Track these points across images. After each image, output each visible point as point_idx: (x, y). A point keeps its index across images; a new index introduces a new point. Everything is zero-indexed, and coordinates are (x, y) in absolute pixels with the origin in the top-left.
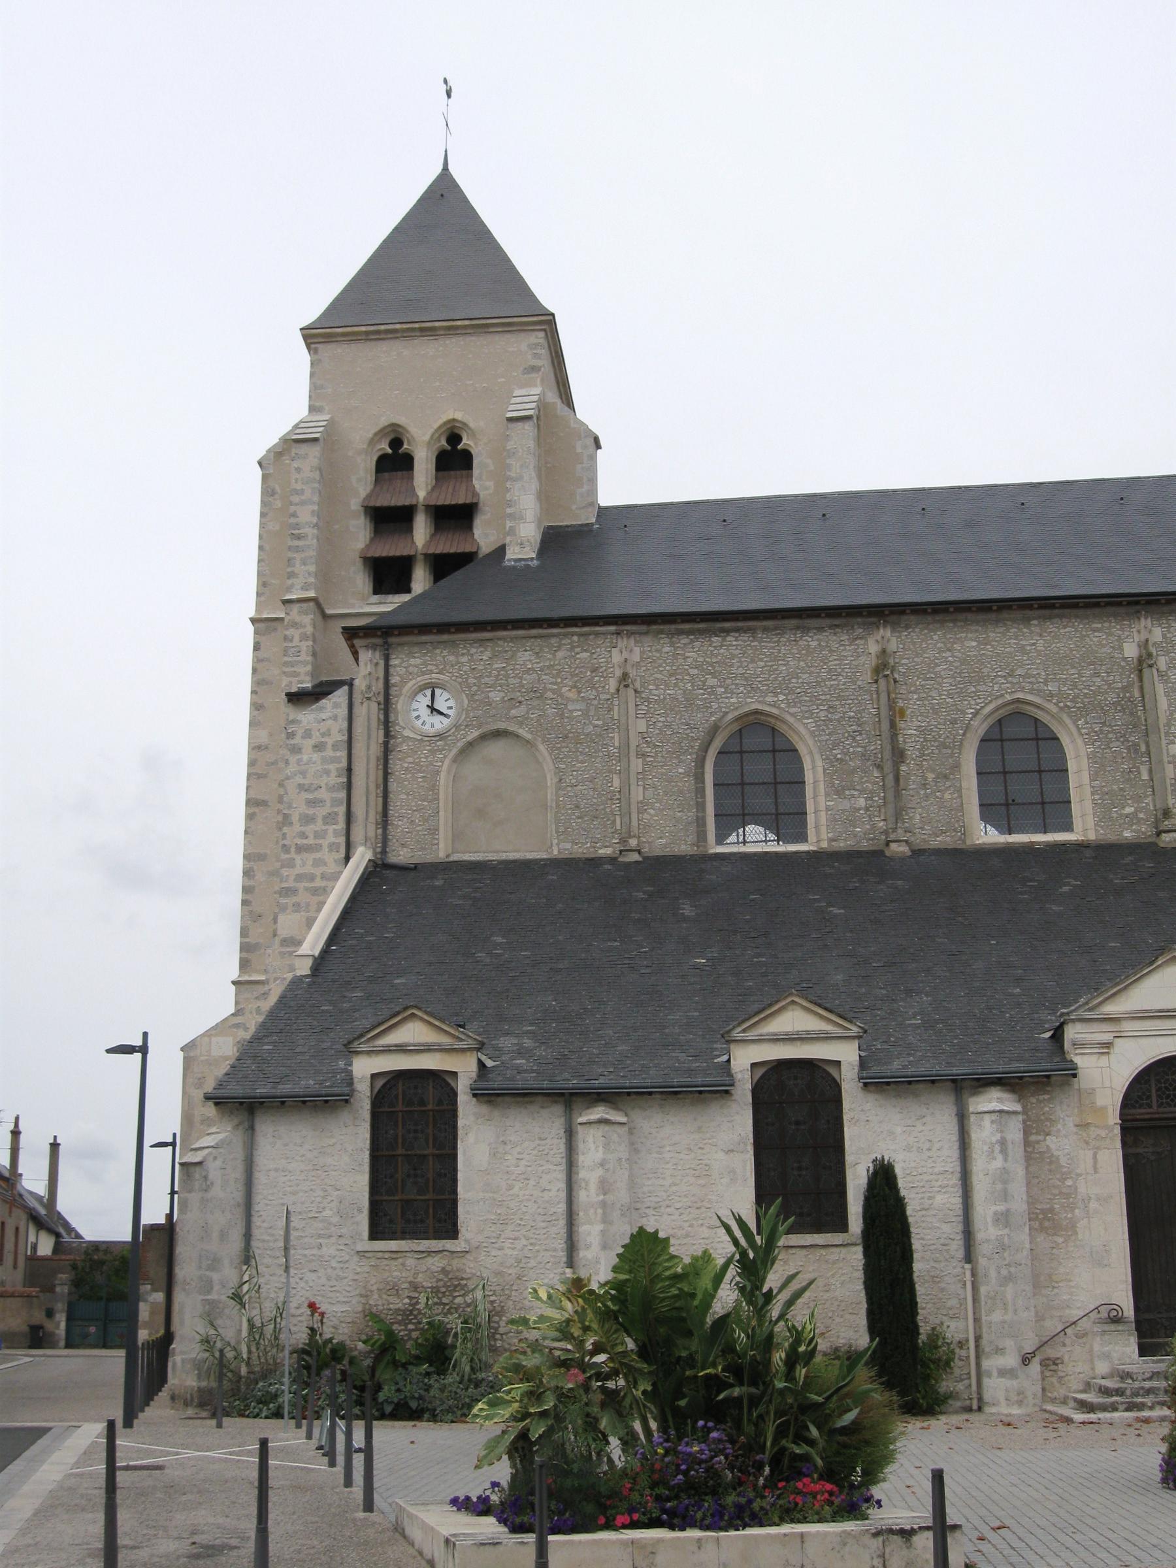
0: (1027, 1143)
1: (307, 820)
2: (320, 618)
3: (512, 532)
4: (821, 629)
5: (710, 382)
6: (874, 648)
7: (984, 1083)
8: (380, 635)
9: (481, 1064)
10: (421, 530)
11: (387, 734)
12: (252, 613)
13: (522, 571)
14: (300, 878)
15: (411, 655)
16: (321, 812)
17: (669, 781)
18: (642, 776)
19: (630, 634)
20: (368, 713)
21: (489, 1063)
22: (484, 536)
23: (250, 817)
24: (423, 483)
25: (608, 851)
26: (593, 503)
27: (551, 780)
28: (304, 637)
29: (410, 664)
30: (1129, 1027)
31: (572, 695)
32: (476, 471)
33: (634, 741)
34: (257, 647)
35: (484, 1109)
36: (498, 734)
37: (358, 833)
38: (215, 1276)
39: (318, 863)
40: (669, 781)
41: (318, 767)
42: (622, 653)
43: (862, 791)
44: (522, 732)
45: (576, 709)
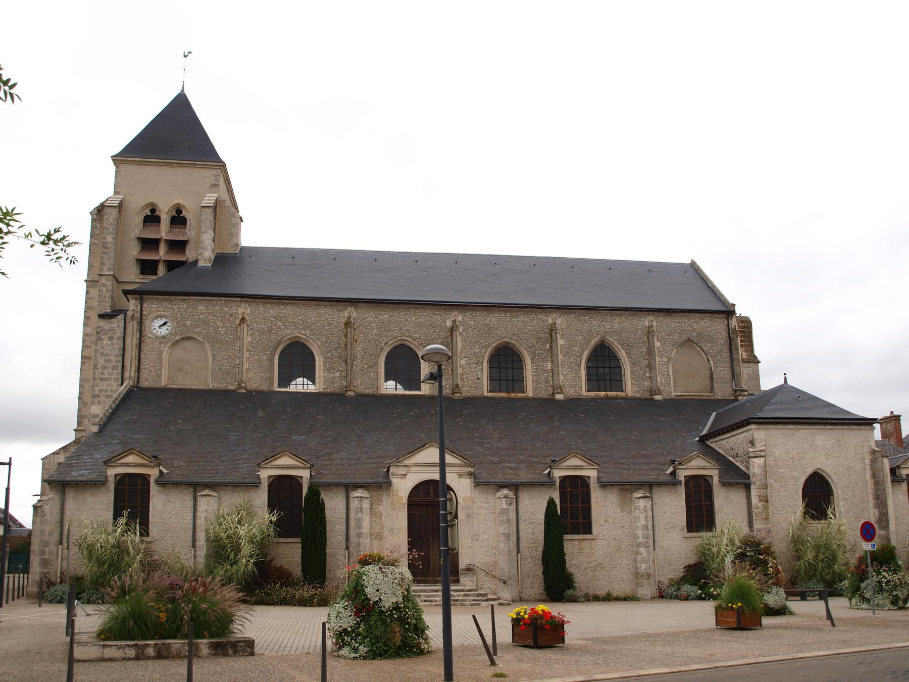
0: (371, 508)
1: (104, 367)
2: (115, 282)
3: (201, 254)
4: (325, 306)
5: (281, 206)
6: (346, 315)
7: (356, 486)
8: (141, 294)
9: (161, 471)
10: (163, 249)
11: (141, 335)
12: (86, 278)
13: (204, 269)
14: (101, 391)
15: (152, 303)
16: (110, 365)
17: (260, 361)
18: (248, 359)
19: (246, 302)
20: (133, 326)
21: (165, 471)
22: (190, 254)
23: (83, 363)
24: (164, 231)
25: (233, 388)
26: (237, 245)
27: (210, 358)
28: (108, 291)
29: (151, 306)
30: (413, 469)
31: (221, 325)
32: (188, 227)
33: (246, 345)
34: (87, 292)
35: (161, 489)
36: (189, 338)
37: (127, 374)
38: (47, 549)
39: (108, 385)
40: (260, 361)
41: (111, 348)
42: (244, 309)
43: (338, 371)
44: (199, 338)
45: (222, 331)
